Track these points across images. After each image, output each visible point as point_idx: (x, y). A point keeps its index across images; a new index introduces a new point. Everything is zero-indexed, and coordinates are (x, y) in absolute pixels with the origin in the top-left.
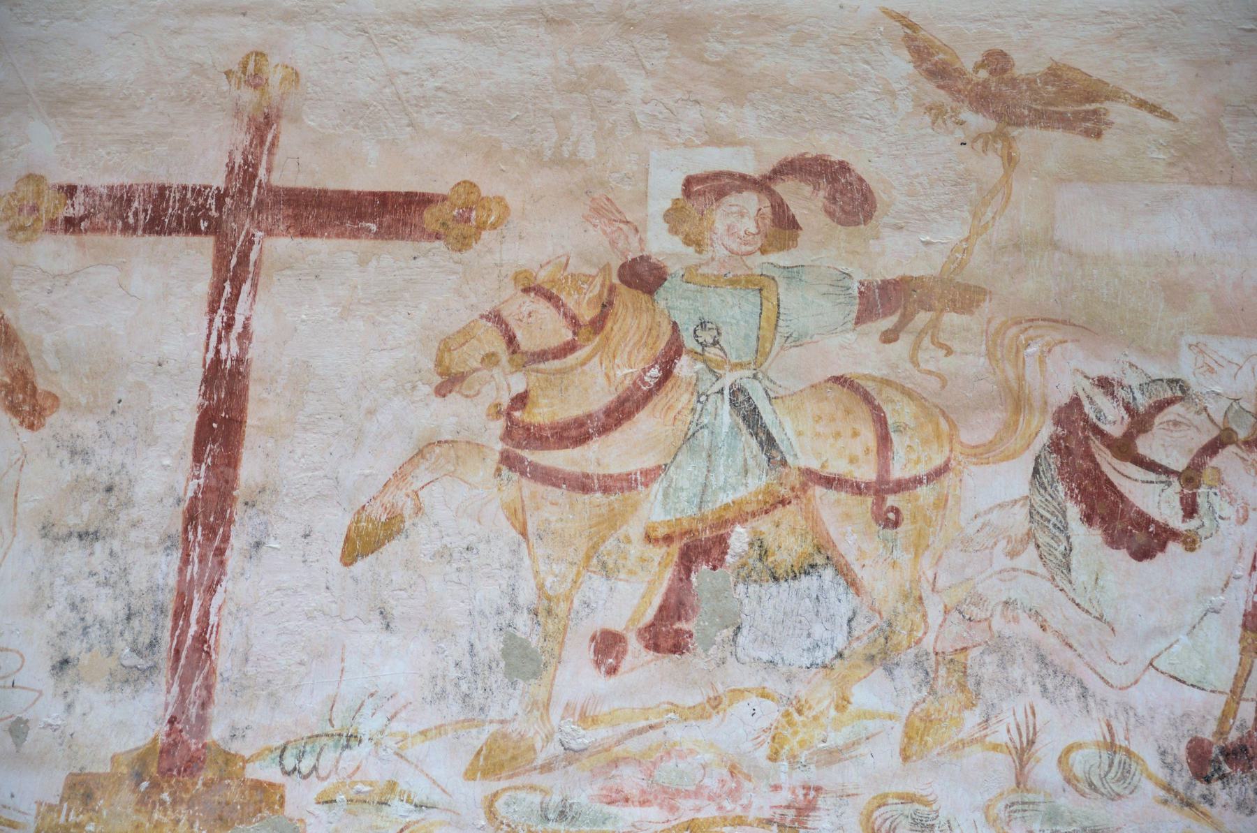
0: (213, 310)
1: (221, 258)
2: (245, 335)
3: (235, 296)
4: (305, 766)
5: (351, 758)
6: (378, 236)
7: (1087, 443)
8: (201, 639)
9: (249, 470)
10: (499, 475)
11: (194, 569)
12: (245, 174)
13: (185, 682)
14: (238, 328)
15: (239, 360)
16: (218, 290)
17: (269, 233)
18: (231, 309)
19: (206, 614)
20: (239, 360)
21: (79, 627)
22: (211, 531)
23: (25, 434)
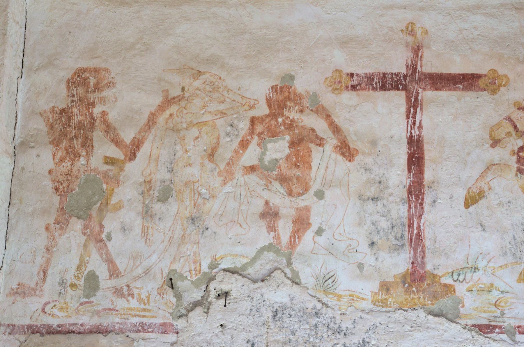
0: (408, 118)
1: (408, 99)
2: (420, 127)
3: (415, 113)
6: (463, 90)
7: (273, 116)
8: (418, 235)
9: (428, 175)
11: (413, 210)
13: (415, 250)
15: (419, 136)
16: (409, 111)
17: (424, 89)
18: (414, 117)
20: (419, 136)
22: (417, 197)
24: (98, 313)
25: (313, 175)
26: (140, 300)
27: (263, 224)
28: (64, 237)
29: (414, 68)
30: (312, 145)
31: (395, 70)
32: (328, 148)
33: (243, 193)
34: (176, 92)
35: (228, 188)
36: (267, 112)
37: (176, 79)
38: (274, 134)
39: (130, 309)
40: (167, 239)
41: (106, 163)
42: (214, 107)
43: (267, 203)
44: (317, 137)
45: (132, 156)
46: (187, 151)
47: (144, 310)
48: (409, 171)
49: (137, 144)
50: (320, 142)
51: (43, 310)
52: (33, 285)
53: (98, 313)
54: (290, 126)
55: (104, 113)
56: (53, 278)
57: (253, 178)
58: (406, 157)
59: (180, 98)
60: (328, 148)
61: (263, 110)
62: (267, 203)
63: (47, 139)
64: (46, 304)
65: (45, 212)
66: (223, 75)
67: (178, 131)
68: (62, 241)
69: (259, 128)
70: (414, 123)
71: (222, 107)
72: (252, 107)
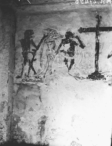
0: (96, 38)
1: (96, 34)
2: (99, 40)
3: (98, 37)
4: (106, 74)
5: (109, 73)
6: (109, 31)
7: (67, 39)
8: (97, 64)
9: (100, 51)
10: (87, 37)
11: (96, 59)
12: (97, 26)
13: (96, 68)
14: (98, 40)
15: (98, 42)
16: (96, 36)
17: (100, 31)
18: (97, 38)
19: (97, 63)
20: (98, 42)
21: (92, 54)
22: (97, 56)
23: (82, 49)
24: (57, 57)
25: (75, 52)
26: (40, 79)
27: (64, 63)
28: (25, 66)
29: (97, 35)
30: (75, 45)
31: (94, 27)
32: (78, 46)
33: (60, 56)
34: (46, 35)
35: (57, 55)
36: (65, 38)
37: (46, 31)
38: (67, 43)
39: (38, 81)
40: (45, 66)
41: (33, 51)
42: (54, 37)
43: (65, 58)
44: (76, 43)
45: (38, 49)
46: (49, 48)
47: (41, 81)
48: (96, 51)
49: (39, 46)
50: (77, 44)
51: (22, 81)
52: (20, 76)
53: (57, 57)
54: (70, 41)
55: (32, 40)
56: (24, 74)
57: (62, 53)
58: (95, 47)
59: (47, 36)
60: (78, 46)
61: (64, 38)
62: (65, 58)
63: (21, 46)
64: (23, 79)
65: (21, 61)
66: (56, 30)
67: (47, 43)
68: (25, 67)
69: (64, 42)
70: (97, 39)
71: (56, 37)
72: (62, 37)
